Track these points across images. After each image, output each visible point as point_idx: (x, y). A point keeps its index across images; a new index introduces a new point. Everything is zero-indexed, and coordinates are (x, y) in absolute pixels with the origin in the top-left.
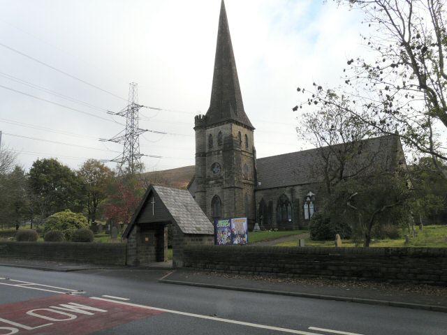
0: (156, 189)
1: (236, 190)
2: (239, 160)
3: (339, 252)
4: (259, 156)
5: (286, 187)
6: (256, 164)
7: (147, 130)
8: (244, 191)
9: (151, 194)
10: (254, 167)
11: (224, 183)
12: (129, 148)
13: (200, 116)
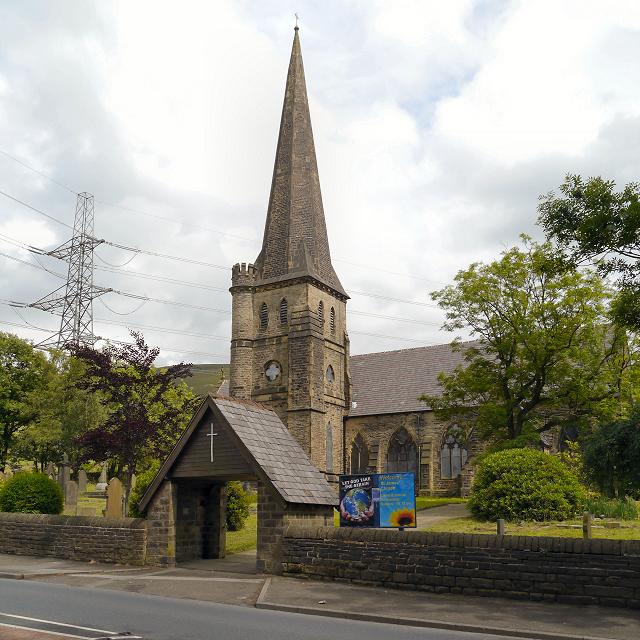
0: (220, 407)
1: (313, 414)
2: (320, 357)
3: (419, 542)
4: (354, 350)
5: (407, 414)
6: (348, 368)
7: (110, 290)
8: (326, 419)
9: (209, 414)
10: (345, 373)
11: (289, 401)
12: (72, 322)
13: (244, 266)
